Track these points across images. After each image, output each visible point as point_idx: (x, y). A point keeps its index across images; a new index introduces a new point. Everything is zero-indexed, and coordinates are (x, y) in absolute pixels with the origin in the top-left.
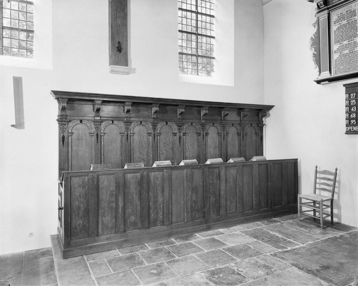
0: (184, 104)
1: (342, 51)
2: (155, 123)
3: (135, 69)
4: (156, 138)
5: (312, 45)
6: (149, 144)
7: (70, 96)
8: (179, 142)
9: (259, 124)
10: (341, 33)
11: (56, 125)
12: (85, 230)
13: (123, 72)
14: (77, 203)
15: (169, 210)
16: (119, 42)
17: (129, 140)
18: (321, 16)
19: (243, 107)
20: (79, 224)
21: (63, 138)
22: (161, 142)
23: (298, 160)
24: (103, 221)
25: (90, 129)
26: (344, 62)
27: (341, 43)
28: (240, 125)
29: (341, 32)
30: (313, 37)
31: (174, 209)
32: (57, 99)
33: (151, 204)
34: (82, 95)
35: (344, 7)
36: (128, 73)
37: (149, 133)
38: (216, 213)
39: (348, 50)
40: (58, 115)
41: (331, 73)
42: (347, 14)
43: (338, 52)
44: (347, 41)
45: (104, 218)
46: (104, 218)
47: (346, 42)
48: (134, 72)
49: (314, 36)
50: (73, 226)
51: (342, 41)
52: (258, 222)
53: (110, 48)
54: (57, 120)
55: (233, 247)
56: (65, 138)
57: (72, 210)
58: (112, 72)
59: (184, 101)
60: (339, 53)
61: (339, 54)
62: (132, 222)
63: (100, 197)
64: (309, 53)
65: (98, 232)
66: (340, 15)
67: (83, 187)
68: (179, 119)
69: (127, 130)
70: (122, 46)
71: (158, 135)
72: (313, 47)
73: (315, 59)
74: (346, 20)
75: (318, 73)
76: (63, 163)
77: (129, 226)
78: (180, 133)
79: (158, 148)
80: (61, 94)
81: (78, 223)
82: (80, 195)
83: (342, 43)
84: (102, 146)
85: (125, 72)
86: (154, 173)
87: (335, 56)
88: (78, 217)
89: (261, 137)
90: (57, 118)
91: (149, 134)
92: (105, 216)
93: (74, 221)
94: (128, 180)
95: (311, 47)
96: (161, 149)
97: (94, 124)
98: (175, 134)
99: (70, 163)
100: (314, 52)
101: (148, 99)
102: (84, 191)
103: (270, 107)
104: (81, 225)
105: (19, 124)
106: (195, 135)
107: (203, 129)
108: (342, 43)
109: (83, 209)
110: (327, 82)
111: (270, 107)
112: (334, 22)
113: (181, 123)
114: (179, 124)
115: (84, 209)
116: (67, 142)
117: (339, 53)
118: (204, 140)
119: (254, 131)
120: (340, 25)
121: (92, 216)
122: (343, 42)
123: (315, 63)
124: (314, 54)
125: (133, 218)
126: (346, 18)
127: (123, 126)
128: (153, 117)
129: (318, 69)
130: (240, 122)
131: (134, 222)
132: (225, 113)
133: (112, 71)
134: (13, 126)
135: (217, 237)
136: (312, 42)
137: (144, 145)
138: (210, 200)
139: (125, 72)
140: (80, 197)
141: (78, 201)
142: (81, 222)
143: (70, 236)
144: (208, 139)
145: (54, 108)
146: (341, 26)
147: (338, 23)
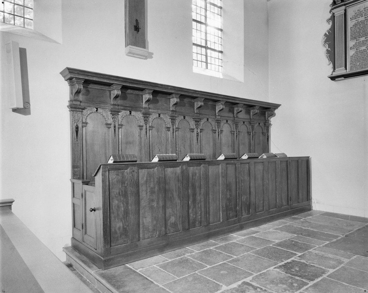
0: (203, 97)
1: (358, 47)
2: (174, 117)
3: (152, 54)
4: (174, 134)
5: (325, 42)
6: (167, 140)
7: (87, 77)
8: (196, 139)
9: (266, 124)
10: (358, 30)
11: (66, 114)
12: (125, 235)
13: (141, 56)
14: (117, 202)
15: (207, 209)
16: (137, 20)
17: (148, 134)
18: (337, 12)
19: (255, 104)
20: (119, 228)
21: (77, 128)
22: (179, 139)
23: (310, 158)
24: (143, 223)
25: (106, 120)
26: (360, 58)
27: (358, 39)
28: (250, 123)
29: (358, 29)
30: (327, 33)
31: (211, 208)
32: (70, 79)
33: (190, 202)
34: (102, 76)
35: (350, 8)
36: (146, 58)
37: (168, 128)
38: (247, 212)
39: (365, 47)
40: (69, 100)
41: (346, 69)
42: (365, 10)
43: (354, 48)
44: (364, 37)
45: (144, 219)
46: (144, 219)
47: (363, 39)
48: (152, 57)
49: (329, 32)
50: (113, 230)
51: (360, 38)
52: (294, 216)
53: (128, 25)
54: (68, 106)
55: (281, 242)
56: (79, 129)
57: (111, 210)
58: (130, 54)
59: (205, 94)
60: (355, 49)
61: (355, 51)
62: (173, 223)
63: (140, 194)
64: (322, 50)
65: (139, 237)
66: (357, 12)
67: (122, 183)
68: (197, 113)
69: (146, 122)
70: (140, 25)
71: (176, 130)
72: (327, 44)
73: (329, 55)
74: (364, 17)
75: (332, 70)
76: (77, 159)
77: (169, 228)
78: (197, 129)
79: (176, 145)
80: (78, 74)
81: (118, 225)
82: (119, 193)
83: (359, 40)
84: (119, 141)
85: (144, 56)
86: (192, 167)
87: (351, 53)
88: (118, 219)
89: (268, 136)
90: (68, 104)
91: (168, 129)
92: (145, 218)
93: (113, 224)
94: (168, 175)
95: (325, 43)
96: (179, 146)
97: (111, 114)
98: (192, 130)
99: (85, 159)
100: (328, 49)
101: (170, 88)
102: (123, 188)
103: (277, 106)
104: (121, 228)
105: (24, 110)
106: (211, 132)
107: (219, 126)
108: (359, 40)
109: (123, 209)
110: (343, 78)
111: (277, 106)
112: (351, 18)
113: (198, 118)
114: (197, 119)
115: (124, 210)
116: (81, 134)
117: (356, 49)
118: (220, 137)
119: (261, 131)
120: (357, 21)
121: (133, 217)
122: (360, 38)
123: (328, 59)
124: (327, 50)
125: (173, 219)
126: (363, 15)
127: (142, 117)
128: (171, 109)
129: (331, 65)
130: (249, 120)
131: (175, 224)
132: (239, 110)
133: (130, 54)
134: (15, 110)
135: (256, 235)
136: (326, 38)
137: (163, 141)
138: (242, 198)
139: (144, 56)
140: (120, 195)
141: (117, 200)
142: (121, 225)
143: (110, 242)
144: (223, 137)
145: (63, 91)
146: (358, 22)
147: (355, 20)
